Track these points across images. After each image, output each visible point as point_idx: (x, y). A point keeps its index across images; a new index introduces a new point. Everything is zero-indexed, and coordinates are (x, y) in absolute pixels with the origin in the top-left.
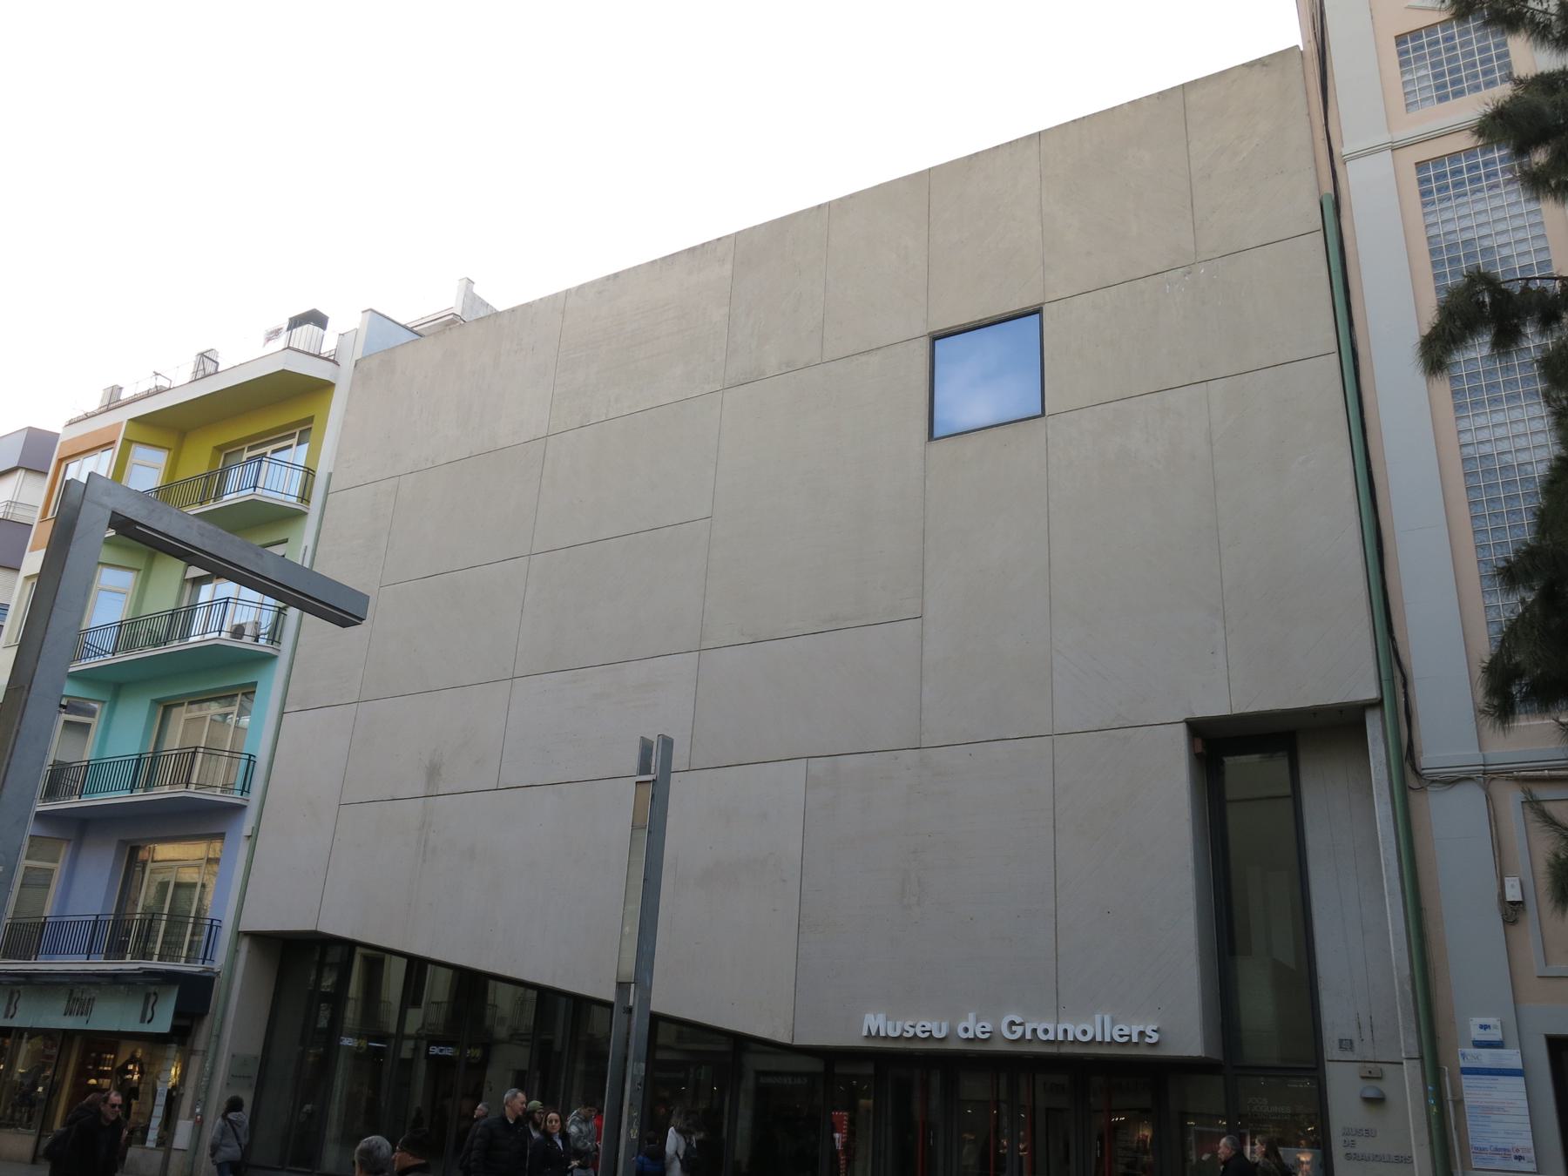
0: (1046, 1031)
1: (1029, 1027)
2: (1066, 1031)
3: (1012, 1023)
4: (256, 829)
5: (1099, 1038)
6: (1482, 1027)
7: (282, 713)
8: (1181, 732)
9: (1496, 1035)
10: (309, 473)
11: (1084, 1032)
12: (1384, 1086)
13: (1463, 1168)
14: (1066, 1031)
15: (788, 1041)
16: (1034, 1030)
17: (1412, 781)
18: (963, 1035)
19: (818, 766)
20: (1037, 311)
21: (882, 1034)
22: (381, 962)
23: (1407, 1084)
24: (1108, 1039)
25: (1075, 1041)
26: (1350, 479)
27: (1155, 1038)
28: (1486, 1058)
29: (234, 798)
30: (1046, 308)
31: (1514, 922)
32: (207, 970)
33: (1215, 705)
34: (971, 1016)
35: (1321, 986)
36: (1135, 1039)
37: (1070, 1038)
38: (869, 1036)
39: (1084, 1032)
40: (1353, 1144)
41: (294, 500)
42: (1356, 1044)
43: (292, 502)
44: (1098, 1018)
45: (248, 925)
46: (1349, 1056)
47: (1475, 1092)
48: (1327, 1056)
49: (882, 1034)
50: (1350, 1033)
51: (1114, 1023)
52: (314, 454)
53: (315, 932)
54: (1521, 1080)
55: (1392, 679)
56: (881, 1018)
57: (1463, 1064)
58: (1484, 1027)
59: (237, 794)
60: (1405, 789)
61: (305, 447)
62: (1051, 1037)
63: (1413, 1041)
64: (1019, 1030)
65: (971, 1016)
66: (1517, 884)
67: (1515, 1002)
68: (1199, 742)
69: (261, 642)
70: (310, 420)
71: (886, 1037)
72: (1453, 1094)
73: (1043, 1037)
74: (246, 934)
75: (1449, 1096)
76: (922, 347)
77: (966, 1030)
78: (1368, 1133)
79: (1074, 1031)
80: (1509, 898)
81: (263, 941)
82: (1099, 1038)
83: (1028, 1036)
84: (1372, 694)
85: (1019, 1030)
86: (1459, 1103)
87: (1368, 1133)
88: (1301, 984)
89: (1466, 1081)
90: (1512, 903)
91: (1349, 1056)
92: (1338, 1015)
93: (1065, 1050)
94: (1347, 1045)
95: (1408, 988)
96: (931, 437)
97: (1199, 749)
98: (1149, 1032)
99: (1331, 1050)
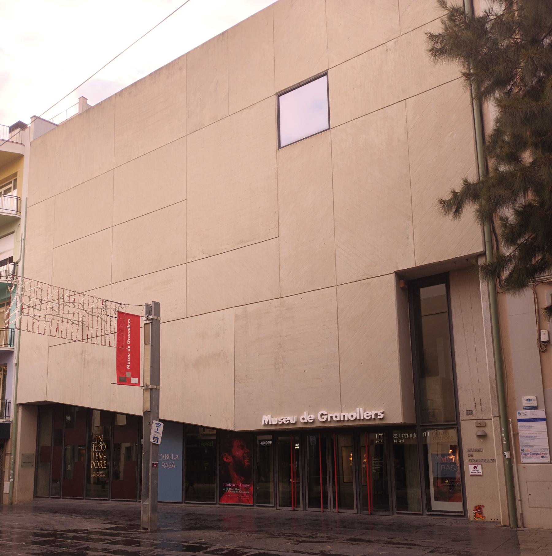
0: (336, 417)
1: (329, 416)
2: (344, 416)
3: (322, 415)
4: (18, 360)
5: (358, 418)
6: (527, 400)
7: (26, 208)
8: (393, 277)
9: (534, 403)
10: (18, 198)
11: (352, 416)
12: (486, 430)
13: (517, 463)
14: (344, 416)
15: (233, 429)
16: (331, 417)
17: (499, 290)
18: (303, 421)
19: (239, 310)
20: (325, 74)
21: (270, 423)
22: (17, 404)
23: (494, 429)
24: (362, 418)
25: (348, 420)
26: (472, 142)
27: (382, 416)
28: (529, 414)
29: (8, 348)
30: (329, 72)
31: (545, 351)
32: (7, 421)
33: (408, 263)
34: (305, 413)
35: (459, 388)
36: (373, 417)
37: (346, 419)
38: (265, 425)
39: (352, 416)
40: (472, 455)
41: (15, 212)
42: (474, 412)
43: (13, 213)
44: (358, 409)
45: (19, 402)
46: (471, 417)
47: (523, 429)
48: (461, 418)
49: (270, 423)
50: (471, 407)
51: (364, 411)
52: (19, 192)
53: (46, 401)
54: (545, 423)
55: (491, 241)
56: (269, 416)
57: (519, 417)
58: (529, 400)
59: (9, 346)
60: (496, 293)
61: (16, 190)
62: (338, 419)
63: (496, 409)
64: (325, 417)
65: (305, 413)
66: (547, 334)
67: (544, 388)
68: (402, 282)
69: (9, 279)
70: (16, 174)
71: (272, 425)
72: (513, 431)
73: (335, 419)
74: (20, 404)
75: (512, 432)
76: (274, 98)
77: (304, 419)
78: (479, 450)
79: (348, 416)
80: (542, 340)
81: (27, 407)
82: (358, 418)
83: (329, 420)
84: (481, 249)
85: (325, 417)
86: (516, 435)
87: (479, 450)
88: (451, 388)
89: (520, 424)
90: (543, 342)
91: (471, 417)
92: (465, 400)
93: (345, 424)
94: (470, 413)
95: (494, 385)
96: (279, 147)
97: (402, 285)
98: (379, 414)
99: (463, 415)
